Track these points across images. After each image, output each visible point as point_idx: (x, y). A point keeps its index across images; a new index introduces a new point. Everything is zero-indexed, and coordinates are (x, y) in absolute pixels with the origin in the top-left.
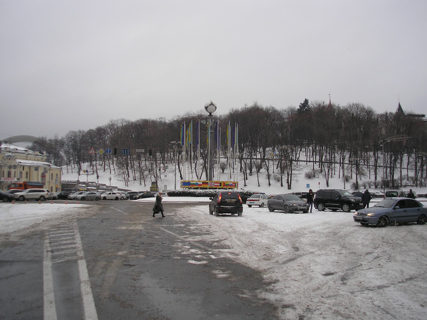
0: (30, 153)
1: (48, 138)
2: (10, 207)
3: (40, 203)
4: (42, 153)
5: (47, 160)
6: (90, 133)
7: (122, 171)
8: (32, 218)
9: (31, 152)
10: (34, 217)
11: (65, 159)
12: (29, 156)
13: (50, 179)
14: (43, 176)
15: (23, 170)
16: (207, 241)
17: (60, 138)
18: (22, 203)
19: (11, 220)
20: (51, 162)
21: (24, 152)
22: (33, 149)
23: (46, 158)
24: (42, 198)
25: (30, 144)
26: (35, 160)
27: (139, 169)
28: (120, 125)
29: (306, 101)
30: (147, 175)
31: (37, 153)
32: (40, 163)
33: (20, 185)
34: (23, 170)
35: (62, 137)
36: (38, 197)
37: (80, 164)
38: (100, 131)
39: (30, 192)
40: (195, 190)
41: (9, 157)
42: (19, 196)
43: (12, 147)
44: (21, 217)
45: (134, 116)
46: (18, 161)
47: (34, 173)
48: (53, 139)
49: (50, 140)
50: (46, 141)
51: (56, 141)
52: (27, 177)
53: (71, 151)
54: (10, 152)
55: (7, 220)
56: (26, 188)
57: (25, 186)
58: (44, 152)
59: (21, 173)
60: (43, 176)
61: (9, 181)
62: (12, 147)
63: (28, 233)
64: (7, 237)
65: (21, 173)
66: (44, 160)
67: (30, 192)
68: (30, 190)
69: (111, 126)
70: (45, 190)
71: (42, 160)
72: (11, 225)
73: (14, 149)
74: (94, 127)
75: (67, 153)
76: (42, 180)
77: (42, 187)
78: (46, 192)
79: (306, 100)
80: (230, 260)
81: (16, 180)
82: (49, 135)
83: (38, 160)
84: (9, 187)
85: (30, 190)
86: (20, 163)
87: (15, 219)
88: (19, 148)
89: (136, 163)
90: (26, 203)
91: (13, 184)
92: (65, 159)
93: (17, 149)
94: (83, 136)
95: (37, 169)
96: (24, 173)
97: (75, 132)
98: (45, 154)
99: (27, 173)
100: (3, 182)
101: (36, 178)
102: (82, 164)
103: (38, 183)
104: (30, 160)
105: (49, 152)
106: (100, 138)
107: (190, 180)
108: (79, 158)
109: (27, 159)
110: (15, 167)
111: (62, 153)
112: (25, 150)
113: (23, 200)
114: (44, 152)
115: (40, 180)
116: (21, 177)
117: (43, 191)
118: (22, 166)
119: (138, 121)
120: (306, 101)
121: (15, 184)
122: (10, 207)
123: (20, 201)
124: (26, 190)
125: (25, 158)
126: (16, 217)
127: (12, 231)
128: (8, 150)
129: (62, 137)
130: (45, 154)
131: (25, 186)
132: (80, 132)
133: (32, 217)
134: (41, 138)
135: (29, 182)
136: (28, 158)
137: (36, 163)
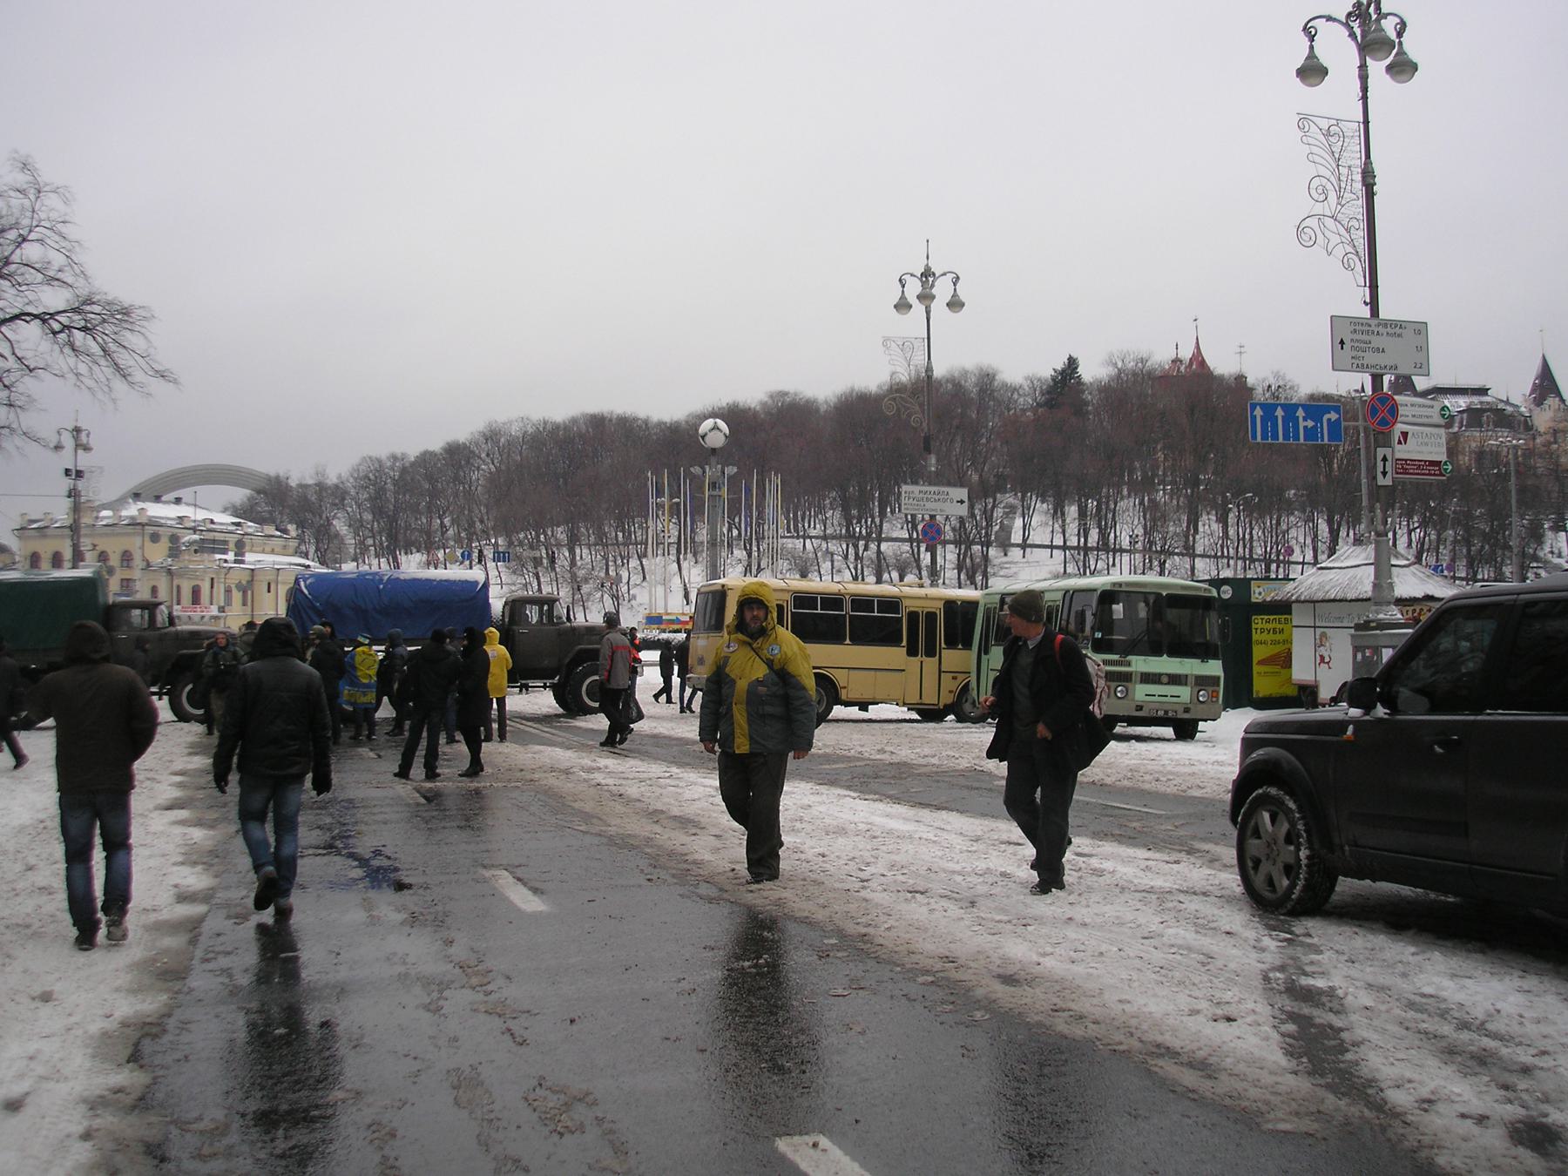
4: (285, 531)
5: (297, 553)
6: (426, 459)
7: (521, 580)
11: (350, 541)
16: (1454, 1067)
17: (332, 479)
25: (239, 495)
26: (263, 552)
27: (568, 576)
28: (515, 430)
29: (1072, 363)
30: (590, 594)
35: (339, 477)
37: (395, 559)
38: (457, 455)
40: (672, 636)
45: (562, 404)
48: (311, 482)
50: (288, 488)
51: (321, 487)
53: (368, 516)
58: (291, 528)
66: (291, 551)
69: (492, 436)
74: (436, 445)
75: (356, 525)
79: (1070, 359)
80: (681, 765)
81: (214, 611)
82: (298, 472)
83: (273, 552)
89: (563, 556)
92: (350, 541)
93: (212, 522)
94: (404, 470)
97: (379, 461)
102: (403, 558)
106: (456, 479)
107: (661, 611)
108: (393, 538)
111: (340, 526)
119: (574, 421)
120: (1072, 363)
129: (339, 477)
132: (394, 458)
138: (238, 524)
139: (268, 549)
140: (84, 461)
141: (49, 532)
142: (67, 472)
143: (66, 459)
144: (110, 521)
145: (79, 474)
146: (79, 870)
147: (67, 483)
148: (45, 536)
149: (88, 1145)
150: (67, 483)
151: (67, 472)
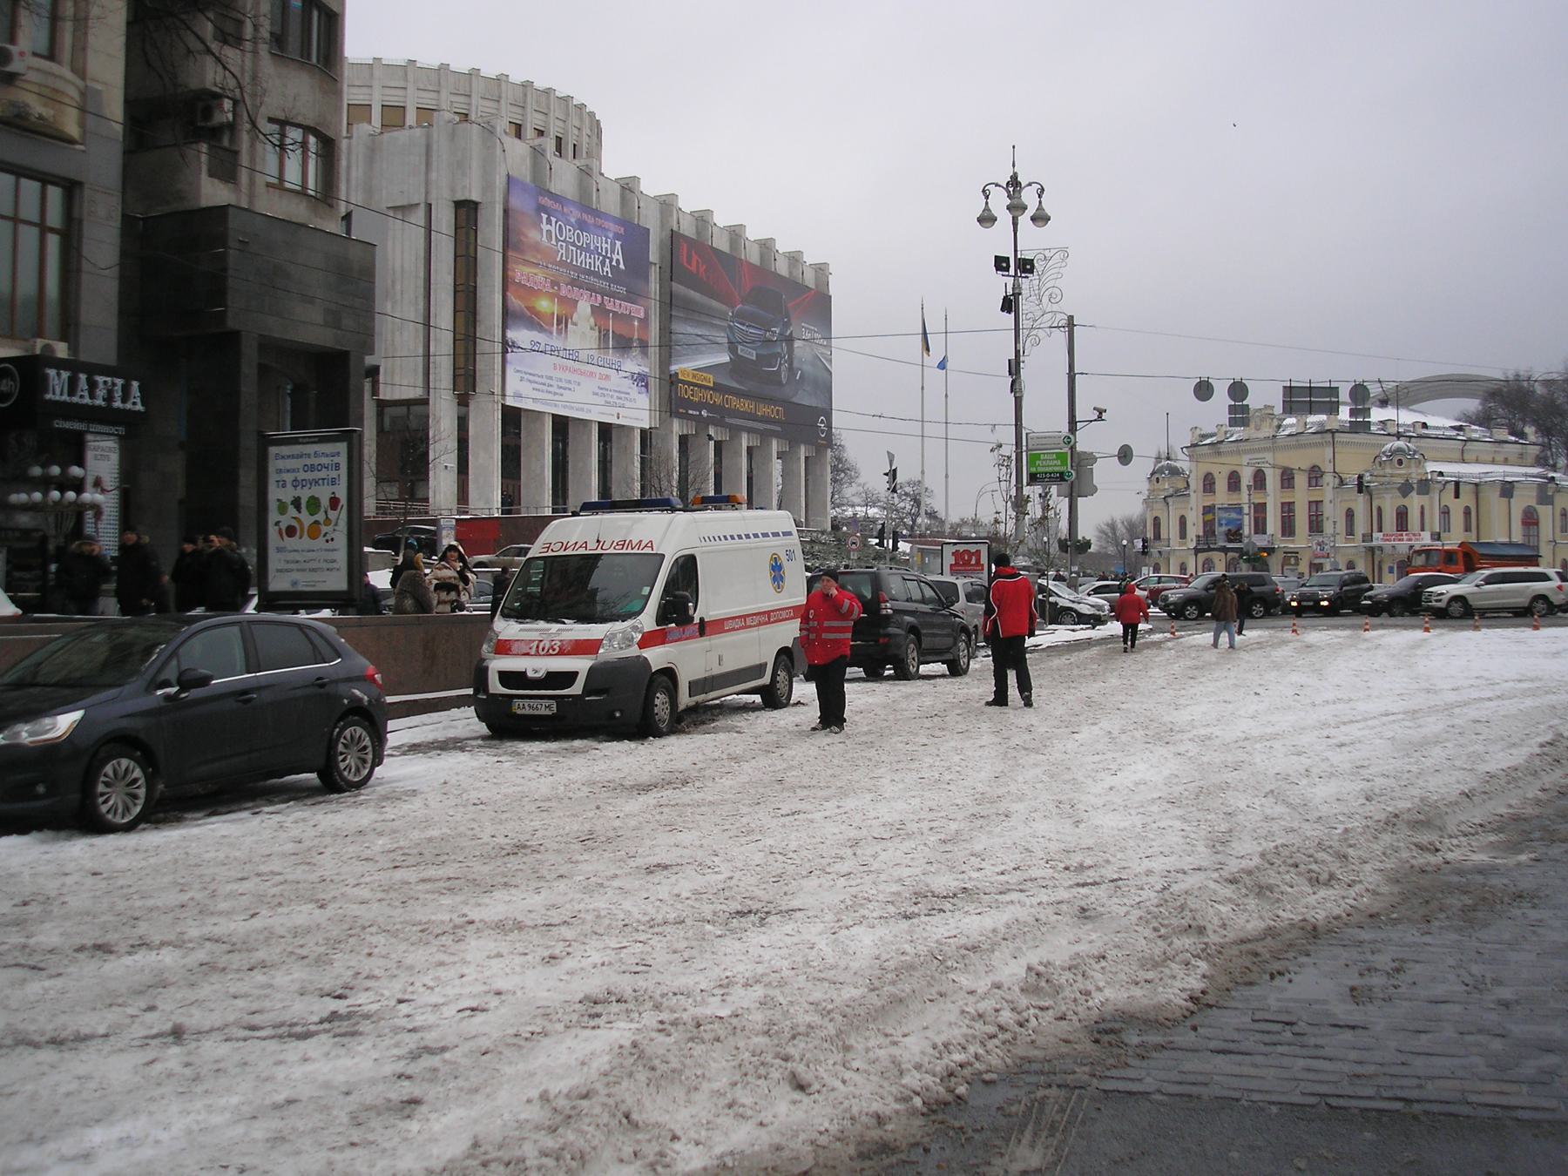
0: (1475, 435)
1: (1539, 373)
2: (1417, 645)
3: (1536, 628)
4: (1522, 435)
5: (1541, 461)
8: (1529, 702)
9: (1476, 432)
10: (1533, 693)
12: (1469, 446)
13: (1558, 529)
14: (1530, 520)
15: (1457, 496)
18: (1462, 628)
19: (1433, 710)
20: (1554, 468)
21: (1454, 433)
22: (1484, 420)
23: (1535, 450)
24: (1456, 608)
25: (1472, 405)
26: (1493, 462)
31: (1503, 434)
32: (1514, 472)
33: (1449, 557)
34: (1457, 496)
36: (1523, 601)
39: (1489, 580)
41: (1398, 457)
42: (1445, 598)
43: (1406, 417)
44: (1475, 695)
46: (1431, 467)
47: (1494, 503)
49: (1547, 383)
52: (1467, 529)
54: (1398, 436)
55: (1413, 714)
56: (1470, 568)
57: (1467, 559)
58: (1530, 430)
59: (1446, 512)
60: (1530, 520)
61: (1403, 545)
62: (1406, 417)
63: (1538, 802)
64: (1425, 838)
65: (1446, 512)
66: (1530, 460)
67: (1489, 580)
68: (1487, 572)
70: (1551, 572)
71: (1521, 460)
72: (1437, 741)
73: (1414, 424)
76: (1527, 535)
77: (1533, 560)
78: (1557, 582)
81: (1426, 539)
83: (1506, 462)
84: (1404, 567)
85: (1487, 572)
86: (1441, 474)
87: (1449, 708)
88: (1430, 421)
90: (1477, 628)
91: (1419, 552)
93: (1425, 425)
95: (1507, 489)
96: (1457, 508)
98: (1532, 438)
99: (1467, 512)
100: (1381, 548)
101: (1501, 528)
103: (1511, 544)
104: (1477, 461)
105: (1546, 431)
109: (1464, 461)
110: (1425, 486)
112: (1453, 428)
113: (1463, 613)
114: (1530, 430)
115: (1517, 537)
116: (1446, 526)
117: (1544, 577)
118: (1451, 487)
121: (1427, 552)
122: (1417, 645)
123: (1452, 618)
124: (1471, 576)
125: (1458, 456)
126: (1452, 697)
127: (1453, 792)
128: (1393, 430)
130: (1532, 438)
131: (1467, 559)
133: (1525, 693)
134: (1511, 377)
135: (1479, 544)
136: (1466, 457)
137: (1498, 472)
138: (1460, 428)
139: (1499, 458)
140: (1032, 240)
141: (1223, 448)
142: (1001, 263)
143: (999, 240)
144: (1293, 430)
145: (1026, 266)
146: (515, 648)
147: (1001, 284)
148: (1219, 453)
149: (158, 1003)
150: (1001, 284)
151: (1001, 263)
